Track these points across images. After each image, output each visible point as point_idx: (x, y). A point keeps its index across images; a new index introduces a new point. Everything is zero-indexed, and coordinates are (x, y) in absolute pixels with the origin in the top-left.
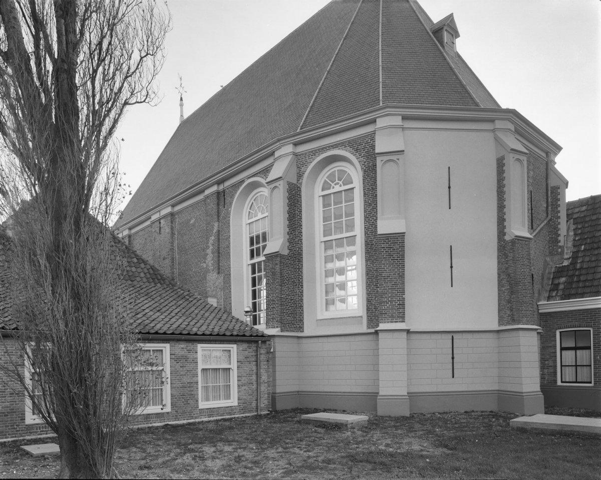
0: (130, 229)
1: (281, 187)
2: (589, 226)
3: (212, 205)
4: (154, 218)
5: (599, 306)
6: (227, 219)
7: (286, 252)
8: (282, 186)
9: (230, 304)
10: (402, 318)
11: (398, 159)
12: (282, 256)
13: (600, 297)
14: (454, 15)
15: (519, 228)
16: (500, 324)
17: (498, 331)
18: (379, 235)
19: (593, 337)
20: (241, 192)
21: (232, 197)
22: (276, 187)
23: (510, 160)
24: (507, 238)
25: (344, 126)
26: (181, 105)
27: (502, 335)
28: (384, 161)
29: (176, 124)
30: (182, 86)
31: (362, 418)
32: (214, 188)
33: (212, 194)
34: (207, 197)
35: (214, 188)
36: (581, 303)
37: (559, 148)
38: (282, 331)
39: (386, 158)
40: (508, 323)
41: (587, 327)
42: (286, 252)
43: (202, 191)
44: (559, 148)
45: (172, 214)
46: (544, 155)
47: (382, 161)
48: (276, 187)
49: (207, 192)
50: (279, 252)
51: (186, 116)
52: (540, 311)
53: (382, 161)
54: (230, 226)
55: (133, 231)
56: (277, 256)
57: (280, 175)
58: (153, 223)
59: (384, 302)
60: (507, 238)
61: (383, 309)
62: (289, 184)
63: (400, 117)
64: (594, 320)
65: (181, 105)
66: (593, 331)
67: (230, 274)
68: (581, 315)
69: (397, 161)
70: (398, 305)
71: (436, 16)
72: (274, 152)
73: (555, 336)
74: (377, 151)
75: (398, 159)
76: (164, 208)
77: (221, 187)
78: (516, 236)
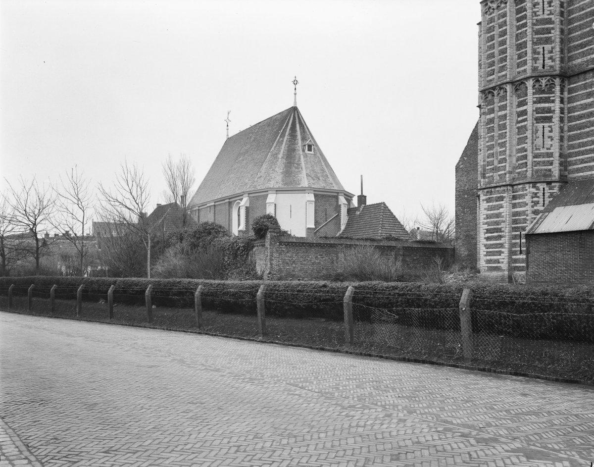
26: (227, 129)
32: (228, 200)
62: (246, 207)
65: (227, 129)
77: (231, 200)
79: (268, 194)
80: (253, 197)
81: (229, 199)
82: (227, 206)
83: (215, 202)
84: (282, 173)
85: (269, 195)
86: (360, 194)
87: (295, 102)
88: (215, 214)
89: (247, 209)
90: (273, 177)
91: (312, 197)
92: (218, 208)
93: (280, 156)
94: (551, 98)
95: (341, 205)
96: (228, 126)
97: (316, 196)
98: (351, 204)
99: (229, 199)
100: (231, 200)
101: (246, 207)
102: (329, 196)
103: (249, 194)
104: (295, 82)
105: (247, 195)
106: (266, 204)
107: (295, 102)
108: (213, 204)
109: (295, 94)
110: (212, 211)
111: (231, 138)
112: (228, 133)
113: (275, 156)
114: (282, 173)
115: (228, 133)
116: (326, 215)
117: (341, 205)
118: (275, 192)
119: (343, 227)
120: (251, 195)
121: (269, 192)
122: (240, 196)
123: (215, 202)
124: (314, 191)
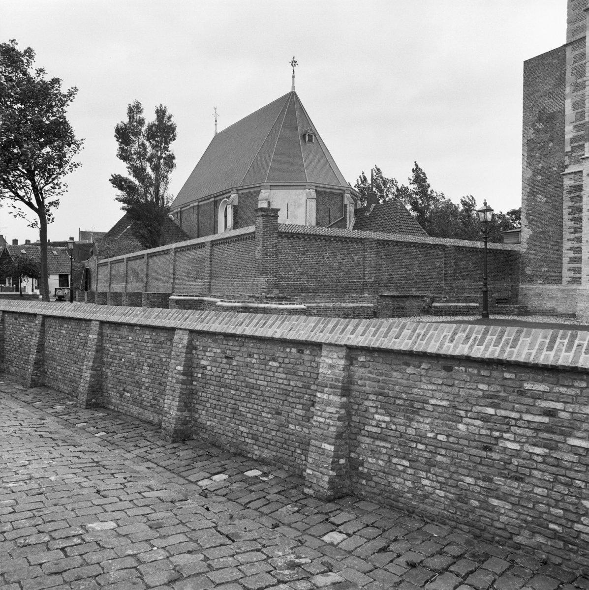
0: (181, 208)
32: (213, 199)
34: (211, 202)
43: (209, 199)
62: (234, 206)
80: (243, 194)
82: (212, 206)
83: (199, 202)
87: (293, 87)
91: (313, 193)
92: (200, 209)
96: (216, 121)
97: (317, 192)
99: (215, 197)
102: (333, 194)
103: (238, 190)
104: (294, 63)
107: (293, 87)
109: (293, 77)
110: (196, 212)
112: (216, 129)
120: (240, 192)
122: (226, 193)
124: (316, 187)
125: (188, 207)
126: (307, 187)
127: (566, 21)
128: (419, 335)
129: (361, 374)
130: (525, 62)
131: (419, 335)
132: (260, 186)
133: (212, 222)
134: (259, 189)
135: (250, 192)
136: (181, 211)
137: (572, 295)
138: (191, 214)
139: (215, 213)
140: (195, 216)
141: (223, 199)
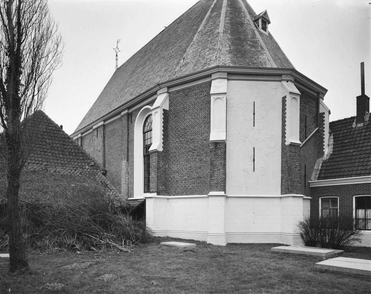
0: (82, 134)
1: (159, 112)
2: (341, 137)
3: (125, 121)
4: (94, 127)
5: (370, 182)
6: (133, 129)
7: (161, 149)
8: (160, 111)
9: (133, 178)
10: (133, 197)
11: (223, 98)
12: (158, 152)
13: (370, 176)
14: (268, 12)
15: (294, 138)
16: (282, 194)
17: (281, 198)
18: (210, 141)
19: (339, 202)
20: (140, 114)
21: (136, 117)
22: (156, 112)
23: (288, 99)
24: (287, 144)
25: (194, 78)
26: (117, 60)
27: (283, 200)
28: (215, 99)
29: (114, 70)
30: (118, 48)
31: (192, 245)
32: (126, 111)
33: (125, 115)
34: (123, 116)
35: (126, 111)
36: (365, 179)
37: (326, 91)
38: (157, 195)
39: (216, 97)
40: (286, 193)
41: (336, 196)
42: (161, 149)
43: (120, 113)
44: (326, 91)
45: (104, 126)
46: (316, 95)
47: (214, 98)
48: (156, 112)
49: (123, 113)
50: (156, 149)
51: (119, 66)
52: (311, 186)
53: (214, 98)
54: (134, 134)
55: (84, 135)
56: (156, 152)
57: (158, 106)
58: (94, 130)
59: (213, 179)
60: (287, 144)
61: (212, 184)
62: (164, 110)
63: (227, 73)
64: (344, 192)
65: (117, 60)
66: (339, 198)
67: (133, 161)
68: (333, 189)
69: (222, 98)
70: (221, 181)
71: (258, 11)
72: (157, 91)
73: (318, 201)
74: (211, 92)
75: (223, 98)
76: (100, 122)
77: (130, 111)
78: (291, 143)
79: (211, 82)
80: (178, 92)
81: (129, 108)
83: (105, 121)
84: (230, 52)
85: (213, 82)
86: (360, 94)
88: (104, 137)
89: (166, 114)
90: (214, 58)
92: (108, 129)
93: (221, 29)
94: (157, 144)
95: (324, 113)
98: (321, 107)
99: (129, 108)
100: (130, 111)
101: (164, 110)
103: (169, 88)
105: (165, 90)
106: (209, 95)
108: (102, 123)
110: (100, 134)
111: (120, 67)
112: (117, 63)
113: (211, 33)
114: (230, 52)
115: (117, 63)
116: (306, 127)
117: (324, 113)
118: (225, 75)
119: (327, 150)
120: (172, 90)
121: (213, 77)
122: (149, 96)
123: (105, 121)
125: (91, 130)
126: (284, 77)
127: (283, 243)
128: (356, 191)
129: (100, 259)
130: (357, 97)
131: (356, 191)
132: (210, 76)
133: (125, 142)
134: (208, 80)
135: (189, 88)
136: (81, 138)
137: (369, 237)
138: (95, 138)
139: (128, 130)
140: (100, 139)
141: (259, 31)
